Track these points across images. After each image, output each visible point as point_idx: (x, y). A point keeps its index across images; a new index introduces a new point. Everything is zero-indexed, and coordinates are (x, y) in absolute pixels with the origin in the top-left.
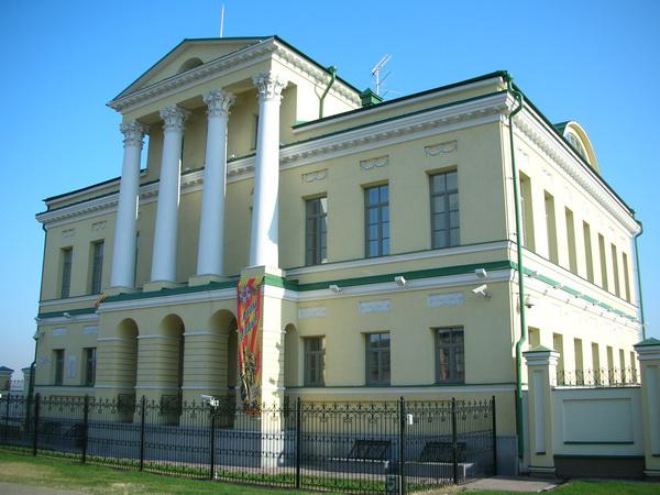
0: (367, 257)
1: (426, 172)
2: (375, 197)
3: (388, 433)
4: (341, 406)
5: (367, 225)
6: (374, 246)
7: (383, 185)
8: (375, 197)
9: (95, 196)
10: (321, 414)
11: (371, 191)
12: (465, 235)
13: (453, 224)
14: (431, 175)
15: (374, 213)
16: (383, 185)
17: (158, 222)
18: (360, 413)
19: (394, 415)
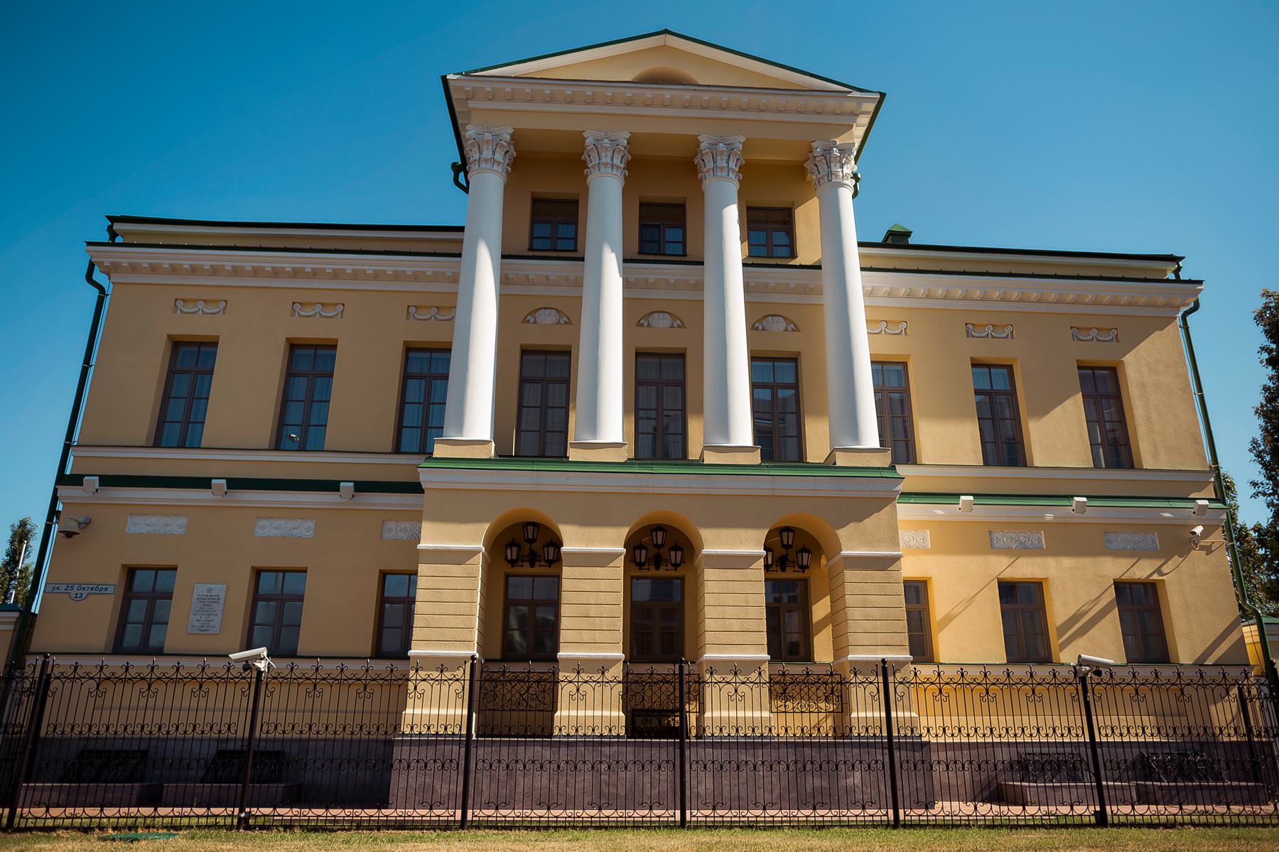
0: (397, 450)
1: (287, 339)
2: (309, 364)
3: (79, 720)
4: (973, 673)
5: (402, 403)
6: (173, 431)
7: (209, 345)
8: (309, 364)
9: (232, 244)
10: (93, 684)
11: (182, 349)
12: (333, 436)
13: (433, 422)
14: (409, 349)
15: (301, 384)
16: (209, 345)
17: (473, 329)
18: (1204, 686)
19: (457, 685)
